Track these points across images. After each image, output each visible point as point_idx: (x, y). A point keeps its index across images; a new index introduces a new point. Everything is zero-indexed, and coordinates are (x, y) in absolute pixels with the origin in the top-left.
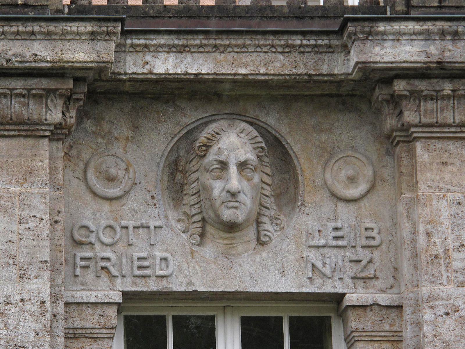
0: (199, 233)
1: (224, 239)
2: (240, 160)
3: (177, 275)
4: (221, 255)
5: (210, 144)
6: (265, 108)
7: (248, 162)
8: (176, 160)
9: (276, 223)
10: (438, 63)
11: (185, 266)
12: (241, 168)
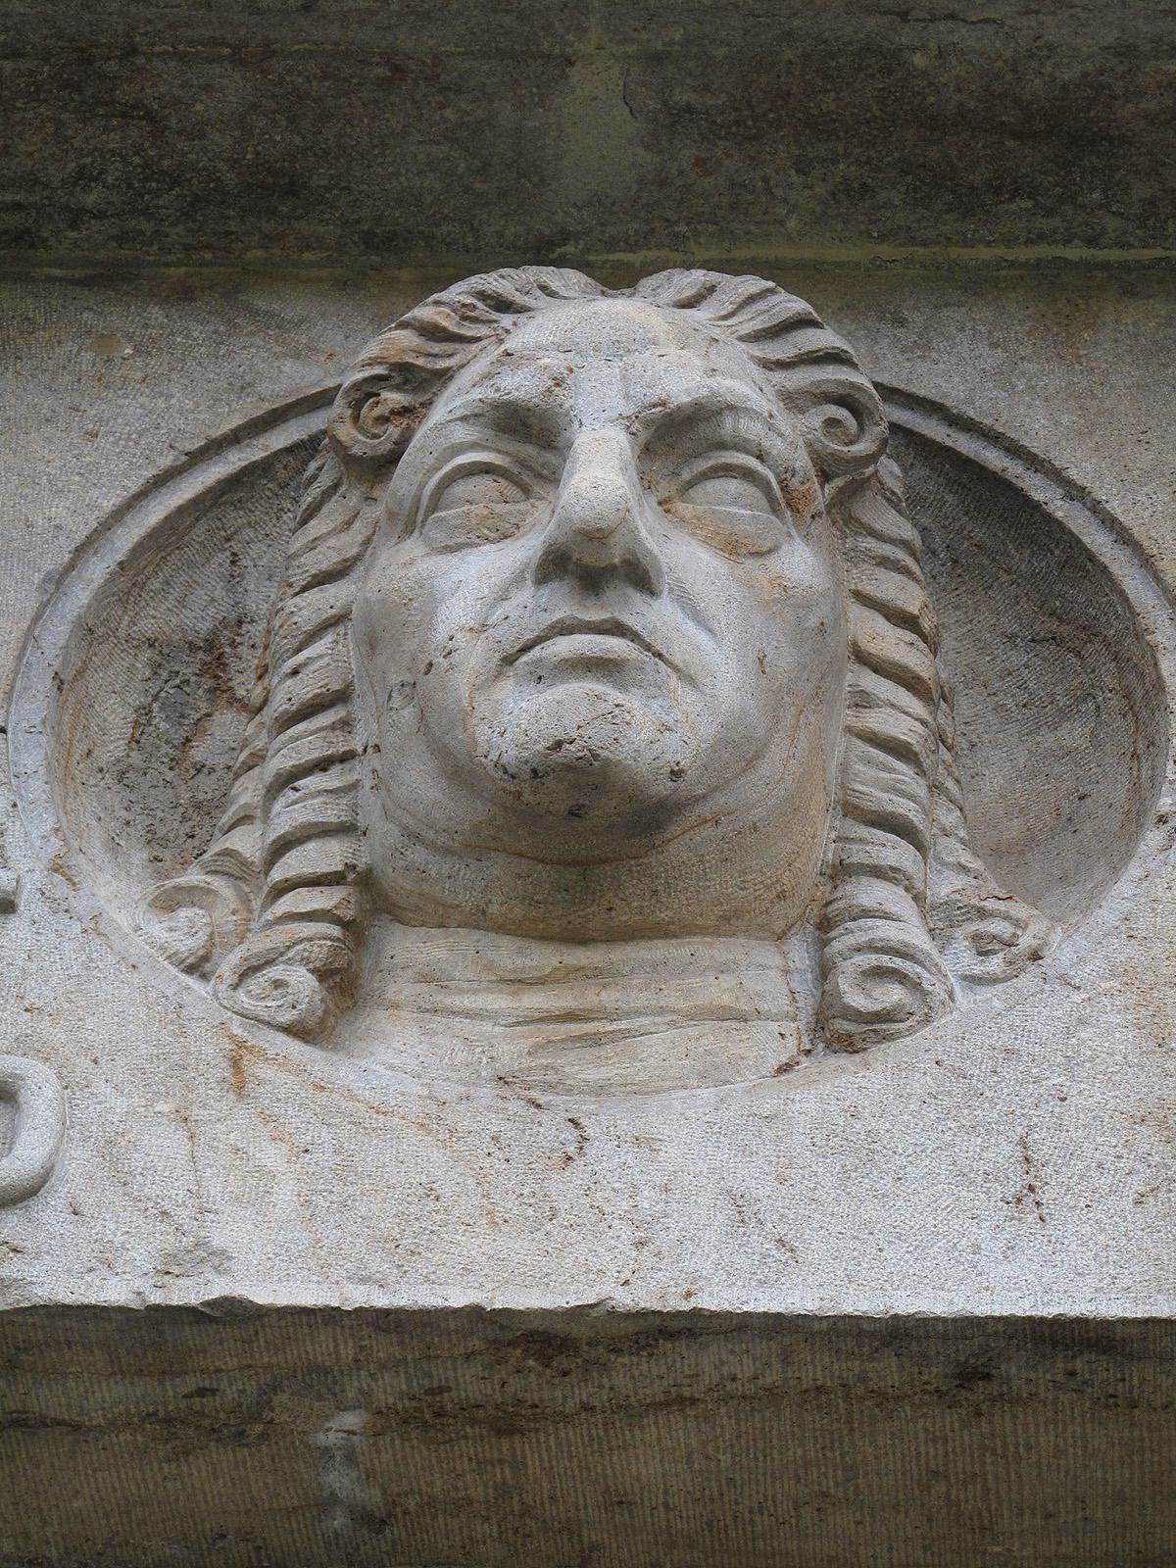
0: (319, 952)
1: (518, 983)
2: (657, 394)
3: (87, 1203)
4: (487, 1093)
5: (441, 364)
6: (902, 323)
7: (728, 422)
8: (214, 632)
9: (976, 937)
11: (164, 1145)
12: (676, 474)
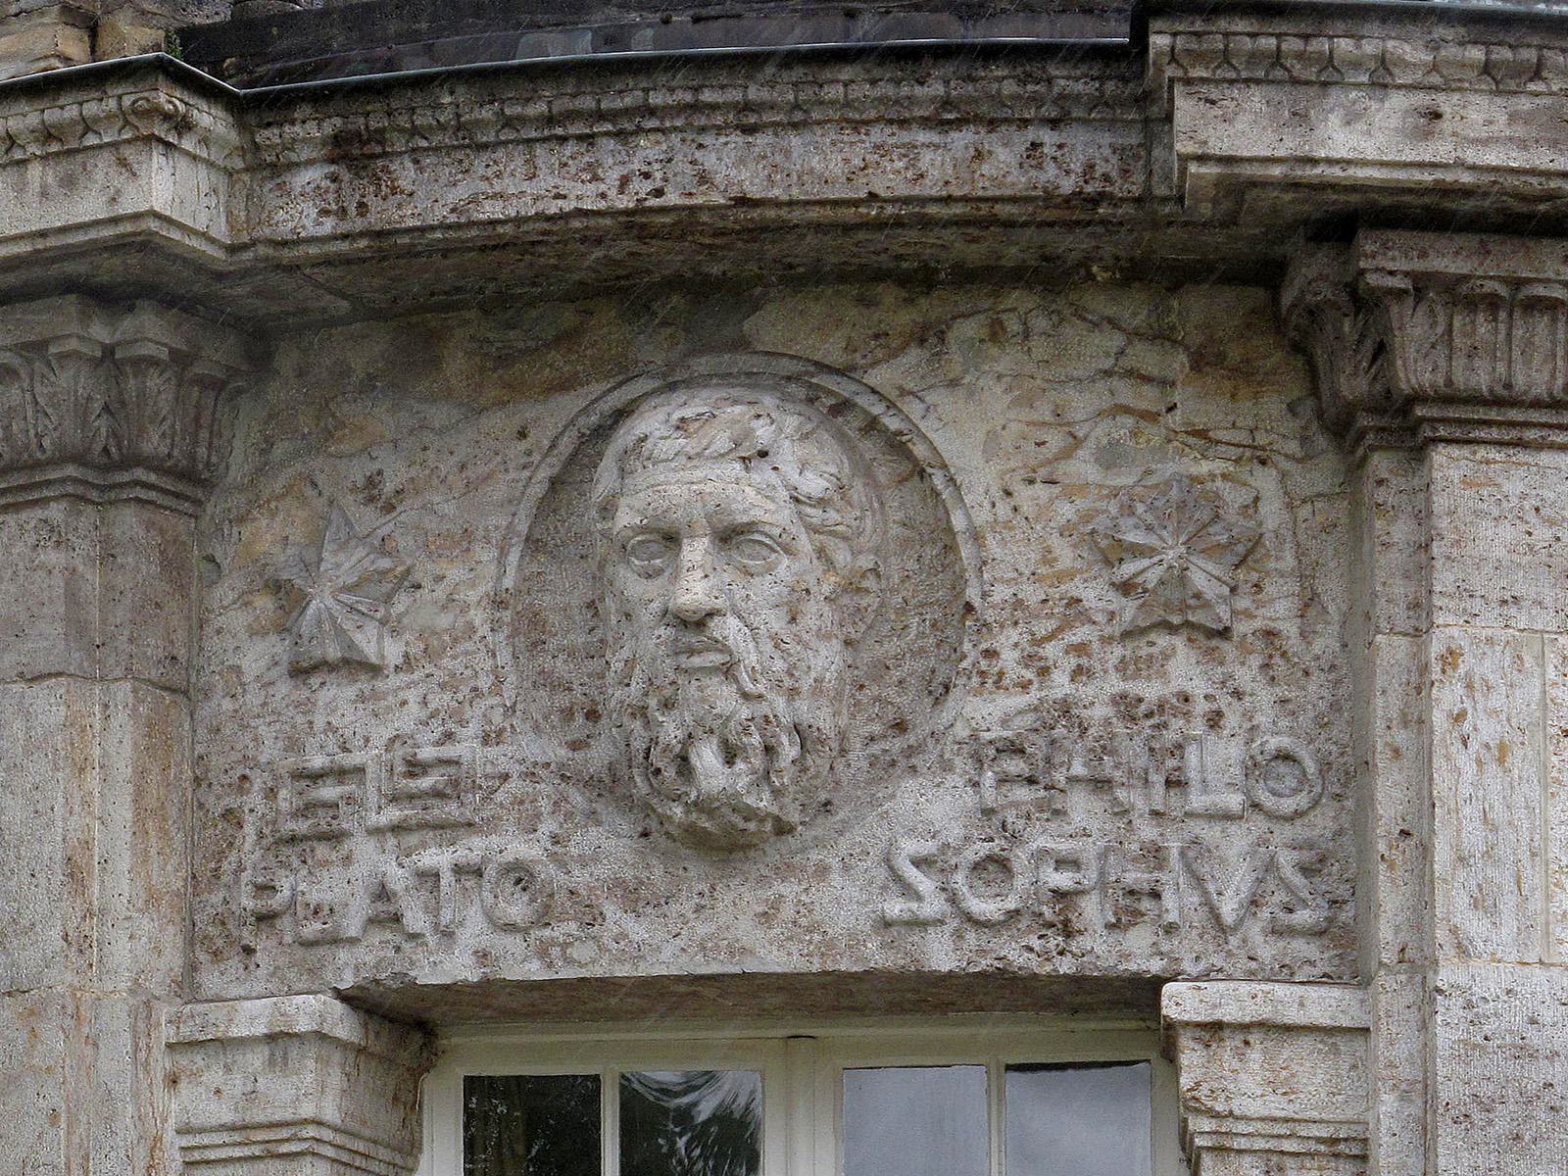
10: (1406, 426)
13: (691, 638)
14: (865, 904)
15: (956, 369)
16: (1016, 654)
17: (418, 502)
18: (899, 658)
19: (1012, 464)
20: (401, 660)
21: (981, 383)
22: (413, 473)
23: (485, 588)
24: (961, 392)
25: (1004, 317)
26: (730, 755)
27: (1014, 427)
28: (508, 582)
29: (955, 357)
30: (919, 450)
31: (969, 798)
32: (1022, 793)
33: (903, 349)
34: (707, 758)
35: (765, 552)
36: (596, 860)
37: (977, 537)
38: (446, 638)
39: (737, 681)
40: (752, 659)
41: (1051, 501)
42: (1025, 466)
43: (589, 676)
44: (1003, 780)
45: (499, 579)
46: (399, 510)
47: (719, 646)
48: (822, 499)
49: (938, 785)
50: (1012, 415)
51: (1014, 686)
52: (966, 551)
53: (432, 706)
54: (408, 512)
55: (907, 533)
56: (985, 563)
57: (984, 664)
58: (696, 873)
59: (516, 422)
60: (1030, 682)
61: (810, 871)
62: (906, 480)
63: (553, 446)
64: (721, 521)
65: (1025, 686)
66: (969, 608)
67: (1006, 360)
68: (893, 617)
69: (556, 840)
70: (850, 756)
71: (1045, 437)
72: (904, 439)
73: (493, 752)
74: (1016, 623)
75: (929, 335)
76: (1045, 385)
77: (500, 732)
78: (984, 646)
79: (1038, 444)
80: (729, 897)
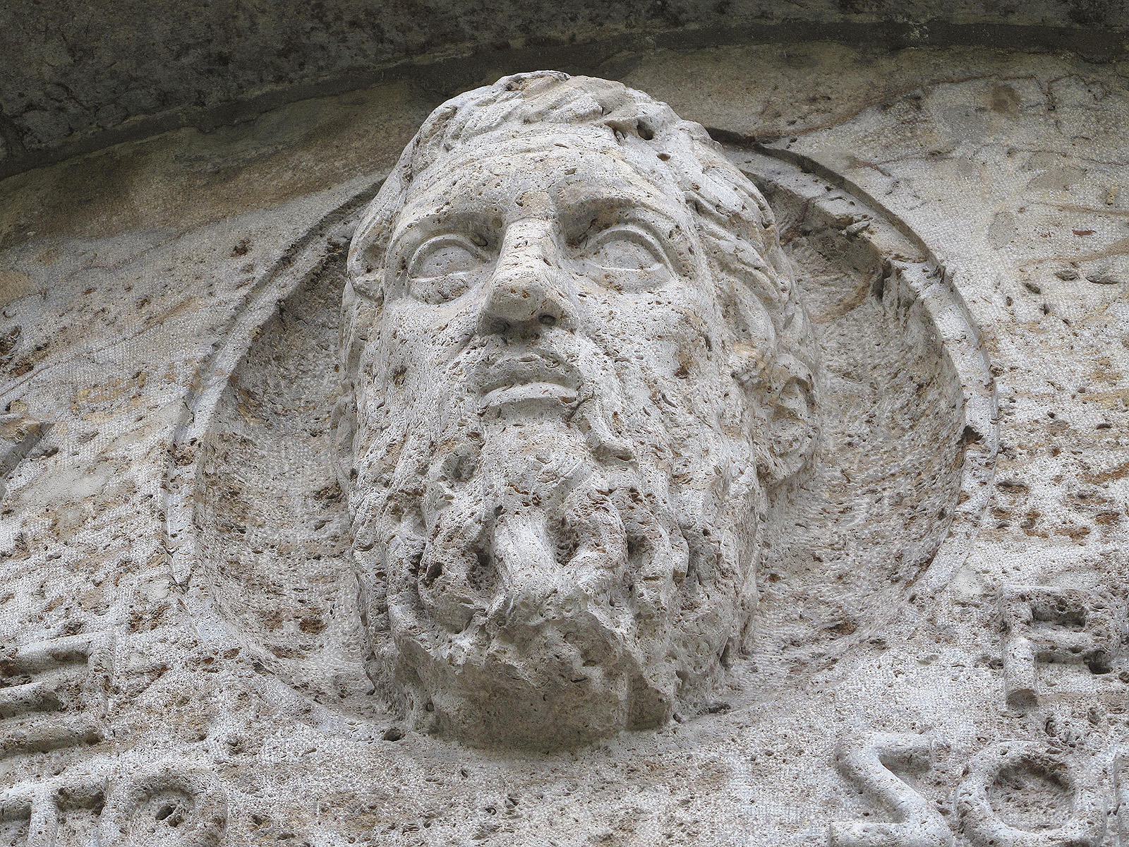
13: (513, 357)
14: (795, 827)
15: (939, 143)
16: (1059, 491)
17: (67, 354)
18: (838, 548)
19: (1038, 254)
20: (12, 545)
21: (982, 157)
22: (66, 321)
23: (163, 434)
24: (948, 168)
25: (1015, 84)
26: (566, 540)
27: (1038, 211)
28: (197, 431)
29: (941, 134)
30: (883, 239)
31: (989, 684)
32: (1080, 681)
33: (853, 115)
34: (524, 544)
35: (643, 255)
36: (304, 770)
37: (982, 340)
38: (89, 506)
39: (586, 428)
40: (613, 399)
41: (1106, 303)
42: (1059, 258)
43: (310, 580)
44: (1046, 658)
45: (182, 427)
46: (36, 369)
47: (561, 370)
48: (736, 215)
49: (926, 662)
50: (1034, 196)
51: (1058, 532)
52: (965, 364)
53: (51, 595)
54: (47, 371)
55: (850, 384)
56: (996, 372)
57: (1003, 500)
58: (485, 778)
59: (234, 238)
60: (1085, 531)
61: (693, 775)
62: (852, 307)
63: (286, 261)
64: (574, 194)
65: (1079, 535)
66: (971, 435)
67: (1022, 134)
68: (826, 496)
69: (236, 747)
70: (757, 658)
71: (1090, 227)
72: (855, 227)
73: (142, 639)
74: (1055, 452)
75: (902, 100)
76: (1084, 165)
77: (158, 614)
78: (1002, 476)
79: (1080, 234)
80: (541, 813)
